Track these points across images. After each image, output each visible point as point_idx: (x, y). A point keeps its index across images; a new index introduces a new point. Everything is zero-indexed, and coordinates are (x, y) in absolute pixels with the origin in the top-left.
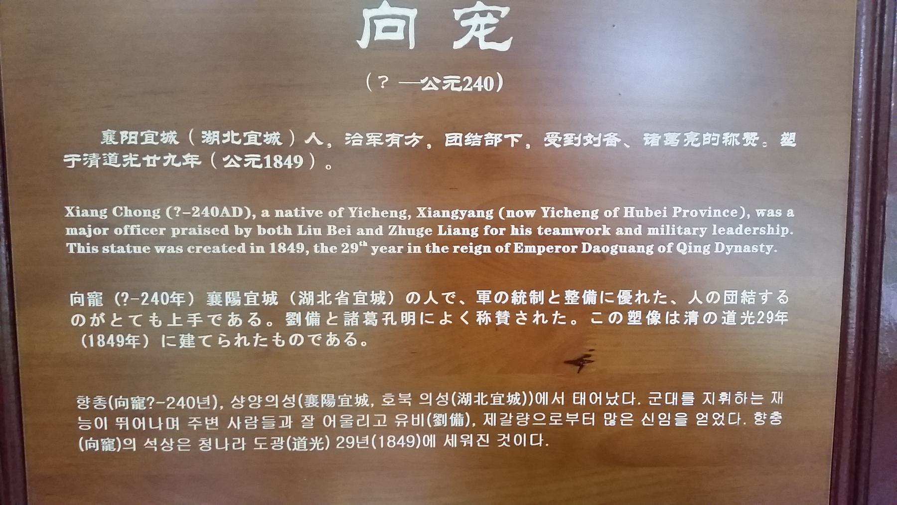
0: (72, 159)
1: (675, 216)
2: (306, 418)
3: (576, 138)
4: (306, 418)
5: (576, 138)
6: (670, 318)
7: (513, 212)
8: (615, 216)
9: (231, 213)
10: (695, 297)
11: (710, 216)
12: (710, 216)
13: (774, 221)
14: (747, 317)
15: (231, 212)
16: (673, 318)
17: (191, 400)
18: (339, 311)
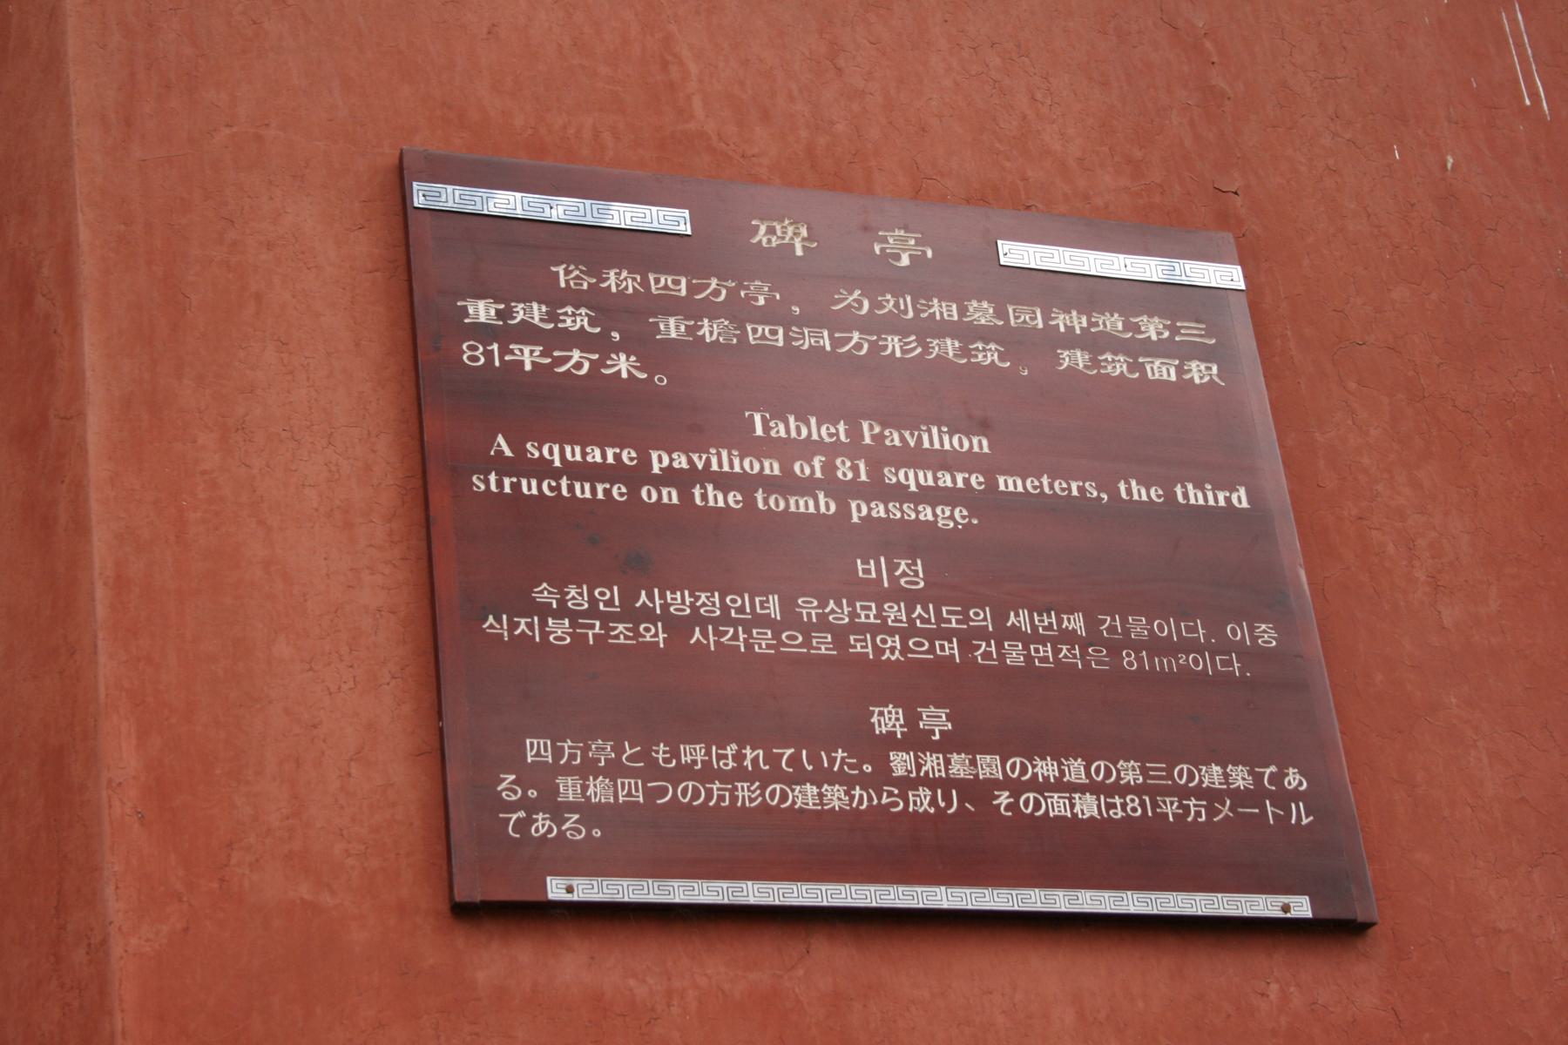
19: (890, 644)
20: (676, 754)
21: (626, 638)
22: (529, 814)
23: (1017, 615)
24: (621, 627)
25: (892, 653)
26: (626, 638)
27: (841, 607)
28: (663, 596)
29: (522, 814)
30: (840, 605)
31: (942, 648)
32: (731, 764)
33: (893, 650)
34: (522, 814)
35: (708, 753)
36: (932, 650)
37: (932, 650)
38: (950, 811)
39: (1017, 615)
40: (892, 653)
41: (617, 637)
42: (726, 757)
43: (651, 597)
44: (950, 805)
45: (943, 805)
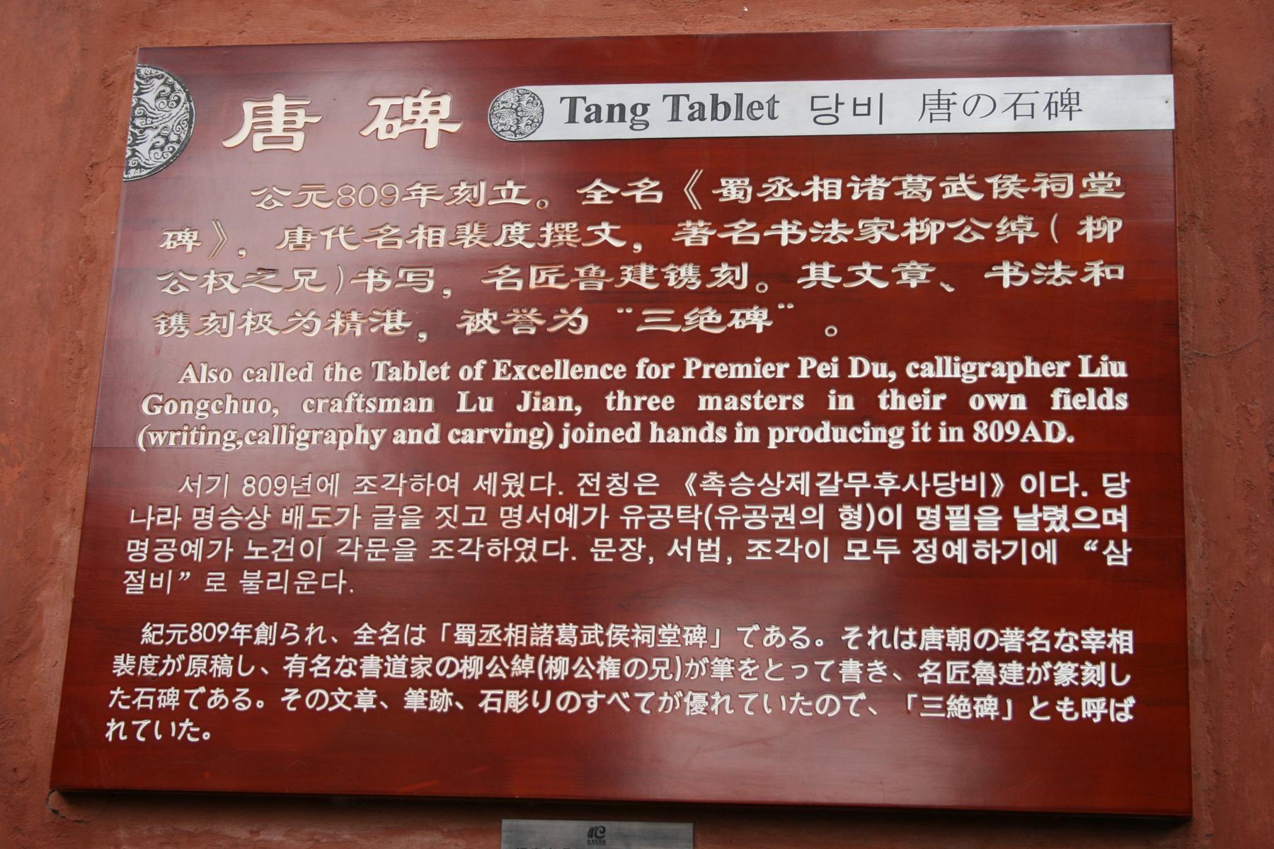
0: (790, 306)
1: (689, 375)
2: (628, 545)
3: (573, 324)
4: (628, 545)
5: (573, 324)
6: (901, 638)
7: (595, 368)
8: (478, 377)
9: (1043, 435)
10: (750, 630)
11: (507, 441)
12: (507, 441)
13: (769, 386)
14: (1065, 706)
15: (1042, 433)
16: (417, 634)
17: (266, 482)
18: (615, 506)
19: (526, 546)
20: (1078, 707)
21: (764, 554)
22: (208, 689)
23: (486, 479)
24: (442, 543)
25: (527, 556)
26: (447, 553)
27: (774, 481)
28: (930, 480)
29: (202, 690)
30: (774, 479)
31: (1110, 517)
32: (912, 645)
33: (528, 552)
34: (202, 690)
35: (1107, 707)
36: (1099, 520)
37: (1099, 520)
38: (541, 711)
39: (486, 479)
40: (527, 556)
41: (755, 554)
42: (1122, 709)
43: (918, 481)
44: (542, 705)
45: (536, 705)
